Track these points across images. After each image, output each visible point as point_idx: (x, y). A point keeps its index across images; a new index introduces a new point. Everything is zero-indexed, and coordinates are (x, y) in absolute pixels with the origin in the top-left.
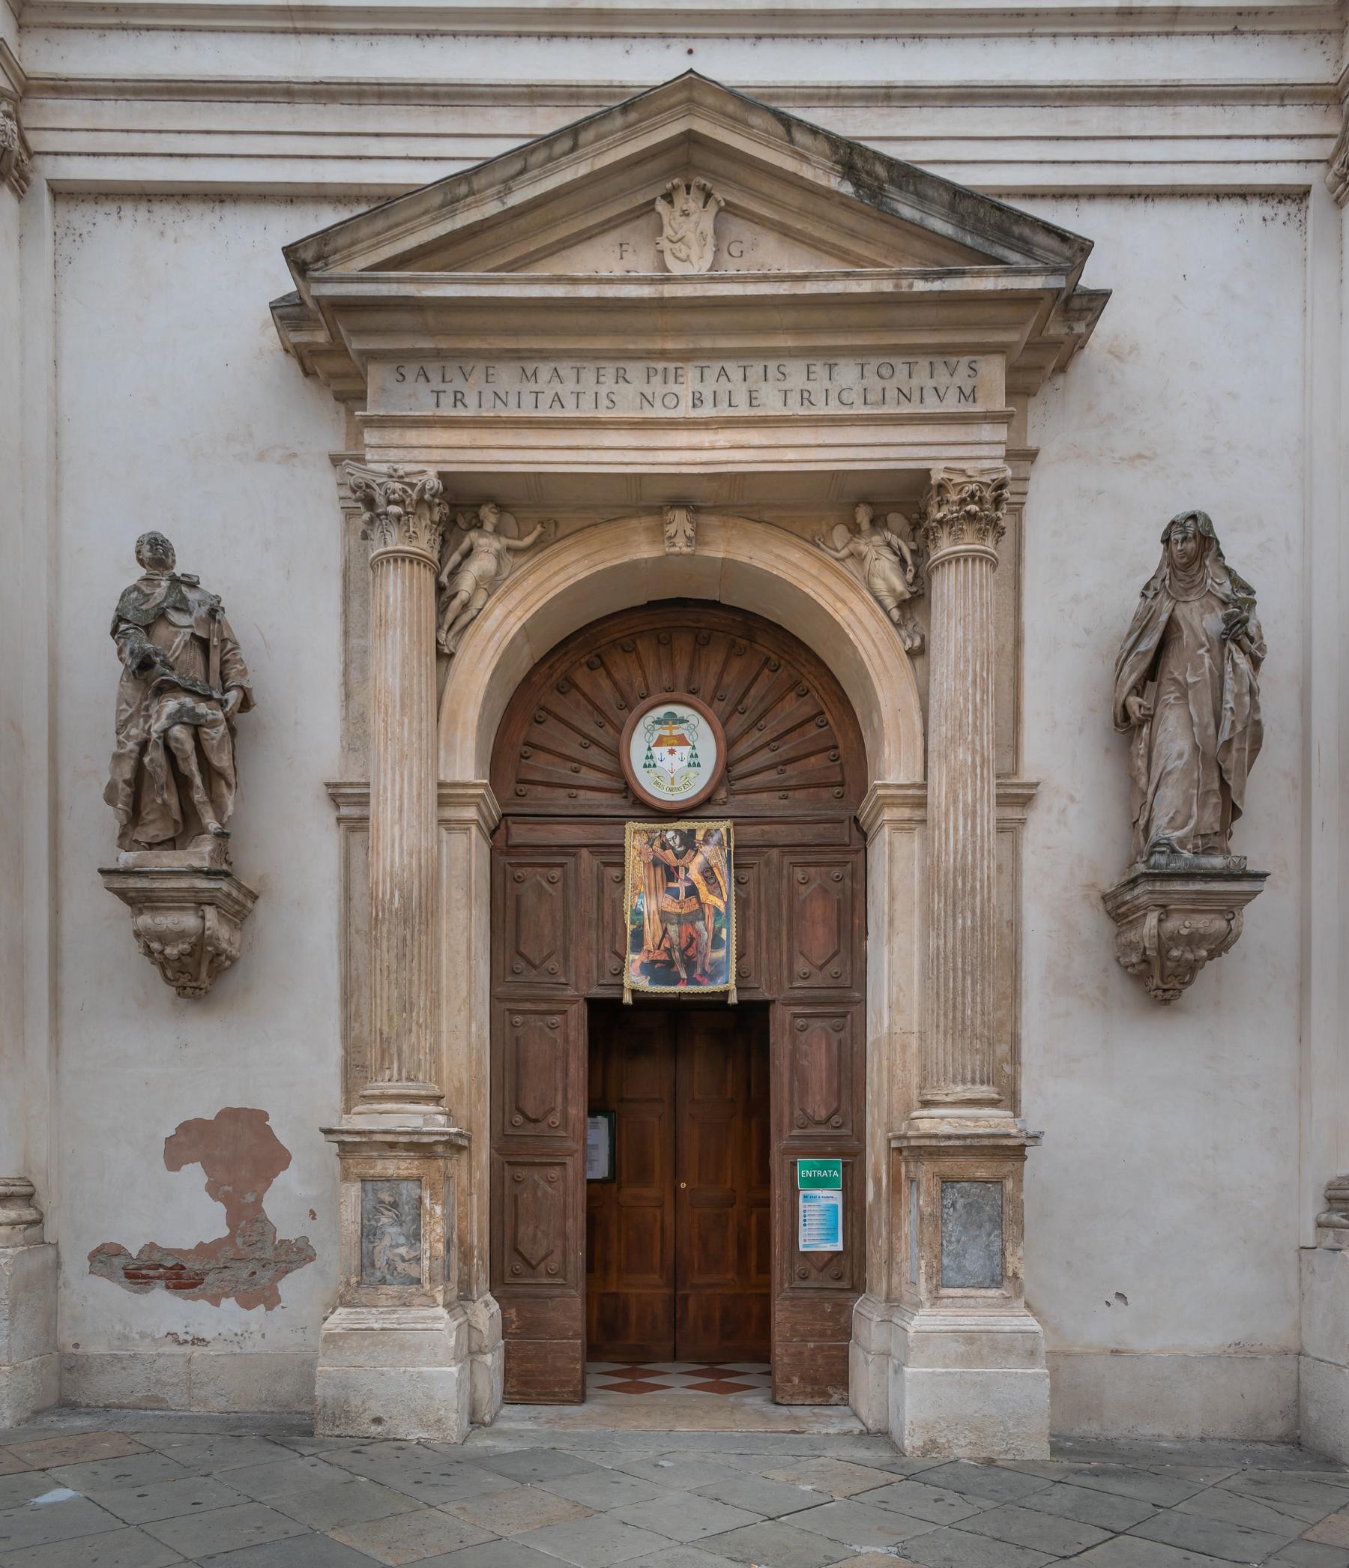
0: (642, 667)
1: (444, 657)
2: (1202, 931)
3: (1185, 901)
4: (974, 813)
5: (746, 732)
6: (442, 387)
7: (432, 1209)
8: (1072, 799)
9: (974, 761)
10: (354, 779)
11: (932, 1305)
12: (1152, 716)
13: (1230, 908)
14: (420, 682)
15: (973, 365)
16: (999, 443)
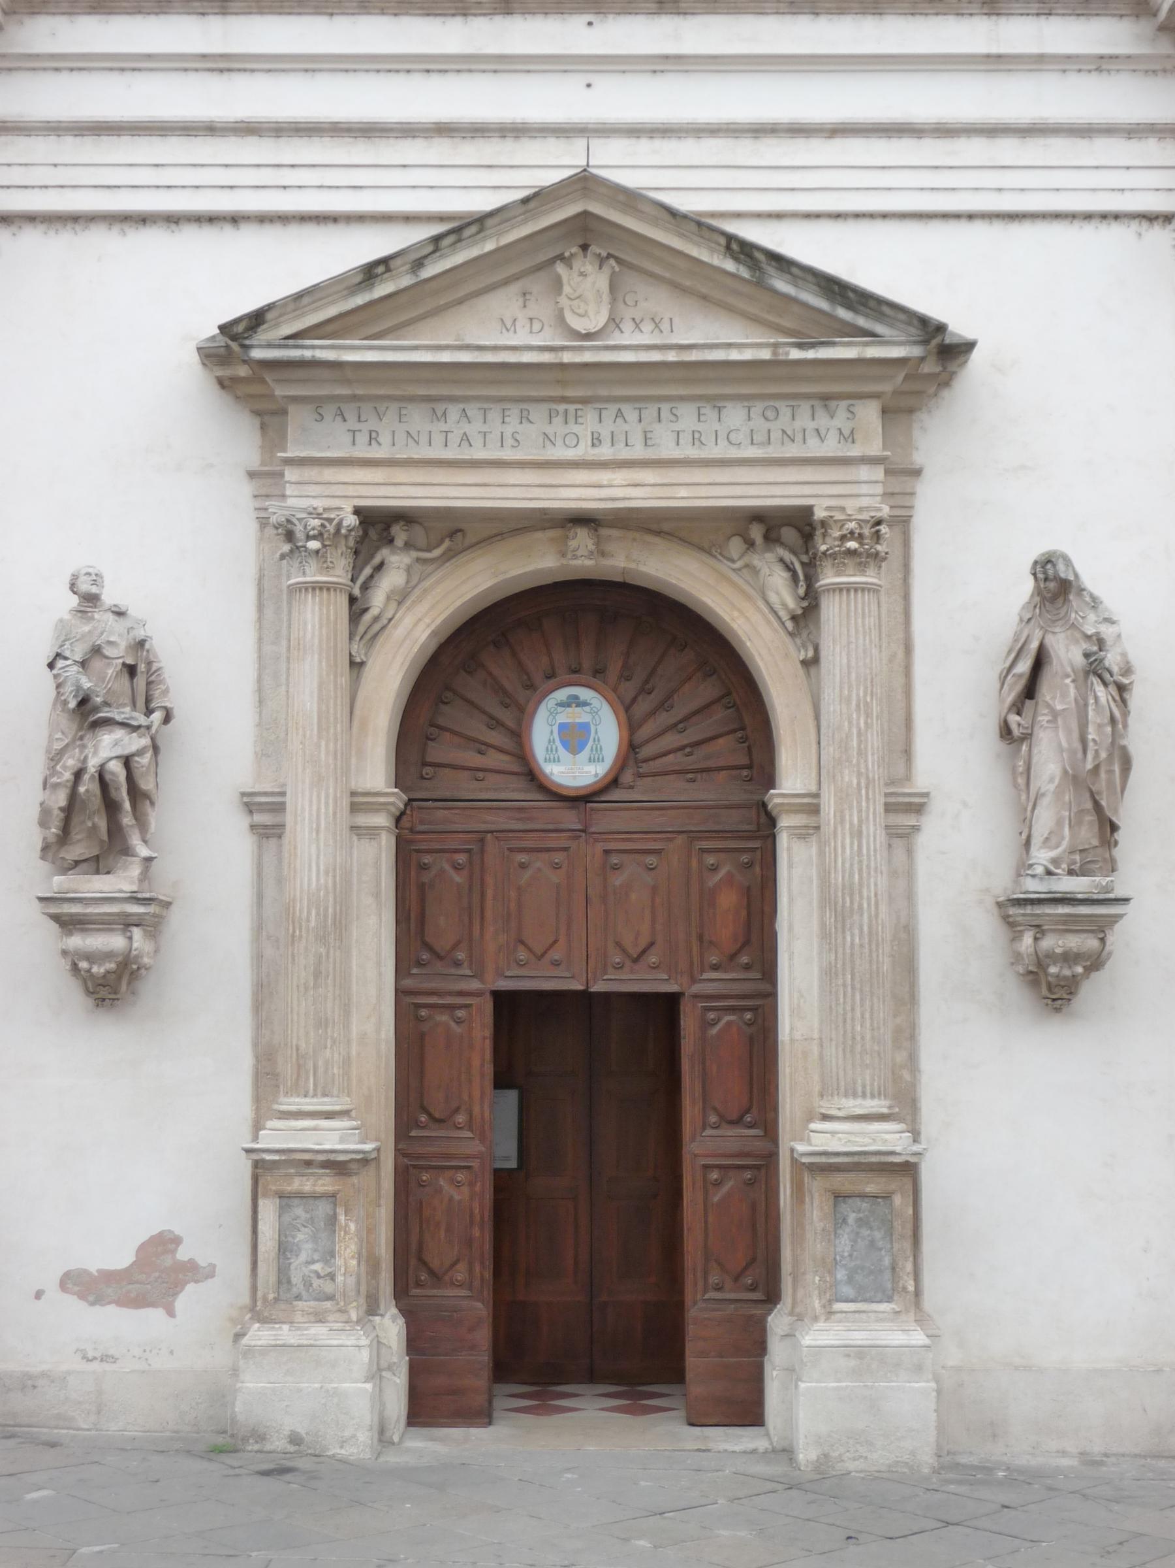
0: (549, 654)
1: (356, 666)
2: (1075, 950)
3: (1057, 923)
4: (860, 833)
5: (653, 713)
6: (357, 426)
7: (346, 1225)
8: (965, 804)
9: (859, 784)
10: (268, 788)
11: (827, 1320)
12: (1031, 735)
13: (1101, 928)
14: (335, 704)
15: (852, 409)
16: (876, 482)
